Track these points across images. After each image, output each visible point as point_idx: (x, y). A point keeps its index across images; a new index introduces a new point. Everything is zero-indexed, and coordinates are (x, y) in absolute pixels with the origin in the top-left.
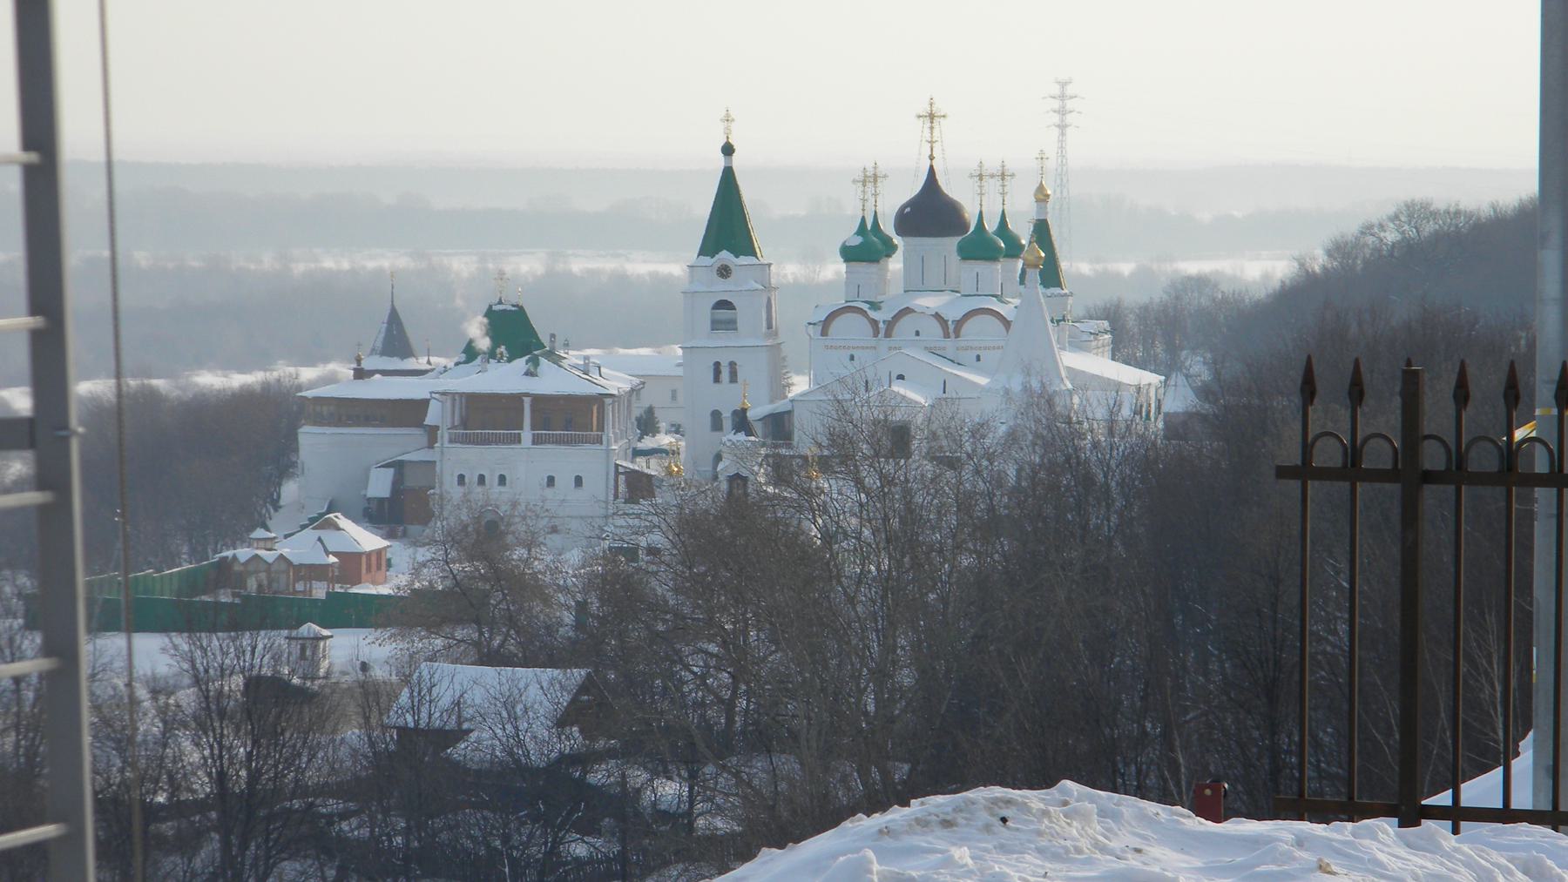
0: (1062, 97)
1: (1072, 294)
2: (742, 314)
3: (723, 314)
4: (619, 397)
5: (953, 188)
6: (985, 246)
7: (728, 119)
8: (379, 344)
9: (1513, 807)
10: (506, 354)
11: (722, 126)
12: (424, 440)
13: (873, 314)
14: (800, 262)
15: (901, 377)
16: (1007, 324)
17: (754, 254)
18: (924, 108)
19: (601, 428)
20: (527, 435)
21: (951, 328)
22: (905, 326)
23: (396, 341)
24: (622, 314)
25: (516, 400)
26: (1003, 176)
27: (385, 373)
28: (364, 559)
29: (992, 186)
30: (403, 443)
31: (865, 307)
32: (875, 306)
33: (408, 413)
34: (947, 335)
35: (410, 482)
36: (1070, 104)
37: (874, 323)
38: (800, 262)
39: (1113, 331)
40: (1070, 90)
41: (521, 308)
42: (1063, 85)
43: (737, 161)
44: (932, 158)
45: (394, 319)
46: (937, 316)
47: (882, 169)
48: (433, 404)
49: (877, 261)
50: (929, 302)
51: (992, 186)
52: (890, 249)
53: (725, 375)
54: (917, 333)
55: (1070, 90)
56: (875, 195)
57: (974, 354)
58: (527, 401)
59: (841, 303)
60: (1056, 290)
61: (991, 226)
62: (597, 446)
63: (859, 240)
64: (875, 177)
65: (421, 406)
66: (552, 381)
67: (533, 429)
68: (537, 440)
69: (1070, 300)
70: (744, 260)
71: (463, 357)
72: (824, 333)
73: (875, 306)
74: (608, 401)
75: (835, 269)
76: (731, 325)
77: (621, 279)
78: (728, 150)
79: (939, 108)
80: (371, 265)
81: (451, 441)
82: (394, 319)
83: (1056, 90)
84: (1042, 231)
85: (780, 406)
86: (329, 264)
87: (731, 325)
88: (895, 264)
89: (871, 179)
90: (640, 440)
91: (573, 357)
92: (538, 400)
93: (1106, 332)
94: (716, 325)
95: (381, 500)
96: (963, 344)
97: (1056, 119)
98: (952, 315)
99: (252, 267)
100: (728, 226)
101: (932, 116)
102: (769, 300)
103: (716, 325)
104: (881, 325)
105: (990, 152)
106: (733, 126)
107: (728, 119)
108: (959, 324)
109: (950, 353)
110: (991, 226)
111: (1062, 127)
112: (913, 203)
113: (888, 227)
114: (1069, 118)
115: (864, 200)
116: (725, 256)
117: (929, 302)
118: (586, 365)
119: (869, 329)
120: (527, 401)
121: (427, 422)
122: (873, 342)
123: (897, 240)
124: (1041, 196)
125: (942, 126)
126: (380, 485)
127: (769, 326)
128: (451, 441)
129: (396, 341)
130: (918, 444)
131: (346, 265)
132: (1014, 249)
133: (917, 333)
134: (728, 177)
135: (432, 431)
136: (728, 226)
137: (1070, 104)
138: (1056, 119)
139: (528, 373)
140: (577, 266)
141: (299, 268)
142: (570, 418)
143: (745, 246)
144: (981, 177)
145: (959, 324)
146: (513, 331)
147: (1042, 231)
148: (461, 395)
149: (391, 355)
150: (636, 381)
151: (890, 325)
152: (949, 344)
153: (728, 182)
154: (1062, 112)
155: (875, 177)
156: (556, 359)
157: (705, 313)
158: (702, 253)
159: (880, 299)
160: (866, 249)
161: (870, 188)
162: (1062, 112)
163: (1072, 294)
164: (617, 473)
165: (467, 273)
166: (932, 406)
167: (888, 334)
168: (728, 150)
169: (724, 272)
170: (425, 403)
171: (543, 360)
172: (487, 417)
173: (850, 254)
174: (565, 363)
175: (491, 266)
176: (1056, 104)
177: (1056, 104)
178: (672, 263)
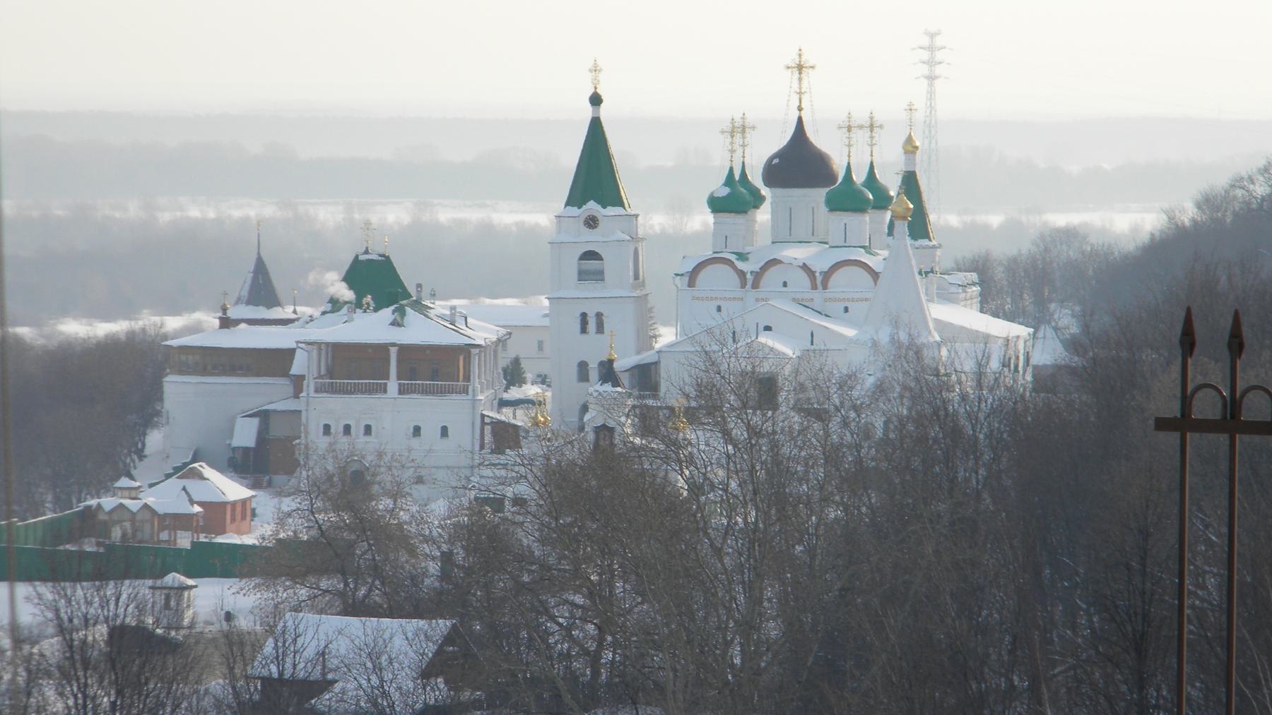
1: (940, 246)
2: (610, 264)
3: (592, 264)
6: (852, 197)
7: (595, 69)
8: (245, 293)
9: (1177, 435)
11: (590, 76)
12: (290, 390)
13: (741, 265)
14: (667, 213)
15: (768, 328)
16: (875, 275)
17: (620, 203)
18: (792, 59)
19: (467, 378)
20: (393, 385)
21: (820, 280)
22: (772, 278)
23: (262, 289)
24: (490, 264)
25: (382, 349)
26: (872, 127)
29: (861, 137)
30: (269, 393)
31: (733, 258)
32: (742, 257)
33: (274, 362)
34: (814, 287)
36: (939, 56)
37: (742, 274)
38: (667, 213)
40: (939, 41)
41: (388, 258)
42: (932, 36)
43: (605, 112)
44: (800, 109)
45: (260, 269)
46: (805, 267)
47: (750, 120)
52: (758, 200)
54: (785, 284)
55: (939, 41)
56: (744, 146)
57: (842, 305)
58: (393, 351)
59: (709, 254)
60: (925, 242)
61: (859, 177)
62: (463, 397)
63: (726, 191)
65: (289, 354)
67: (399, 378)
69: (939, 252)
70: (611, 211)
72: (691, 284)
73: (742, 257)
74: (474, 351)
75: (702, 220)
76: (598, 276)
78: (596, 100)
79: (808, 59)
80: (237, 214)
81: (316, 391)
82: (260, 269)
83: (926, 41)
84: (910, 183)
85: (647, 357)
86: (194, 213)
87: (598, 276)
88: (763, 215)
89: (739, 130)
91: (440, 307)
92: (406, 351)
93: (974, 284)
94: (583, 275)
95: (246, 450)
96: (831, 295)
97: (925, 70)
98: (820, 266)
100: (595, 177)
101: (800, 68)
103: (583, 275)
104: (749, 276)
105: (859, 105)
106: (601, 76)
107: (595, 69)
108: (827, 275)
109: (817, 304)
110: (859, 177)
111: (931, 78)
112: (781, 154)
113: (756, 179)
114: (938, 70)
116: (592, 207)
118: (453, 315)
120: (393, 351)
121: (292, 372)
122: (739, 293)
123: (765, 191)
124: (910, 148)
125: (810, 77)
126: (245, 434)
127: (636, 277)
128: (316, 391)
131: (212, 215)
132: (882, 200)
133: (785, 284)
135: (298, 381)
136: (595, 177)
138: (925, 70)
139: (395, 323)
140: (445, 216)
141: (165, 217)
142: (435, 368)
143: (612, 196)
144: (849, 129)
145: (827, 275)
146: (376, 280)
148: (327, 344)
150: (503, 331)
151: (758, 276)
152: (818, 296)
153: (596, 131)
156: (419, 307)
157: (571, 265)
158: (569, 203)
159: (747, 249)
160: (734, 200)
162: (931, 63)
163: (940, 246)
164: (483, 423)
167: (755, 285)
168: (596, 100)
169: (592, 222)
170: (291, 352)
171: (408, 309)
172: (353, 367)
173: (717, 205)
175: (357, 216)
176: (925, 55)
177: (925, 55)
178: (541, 213)
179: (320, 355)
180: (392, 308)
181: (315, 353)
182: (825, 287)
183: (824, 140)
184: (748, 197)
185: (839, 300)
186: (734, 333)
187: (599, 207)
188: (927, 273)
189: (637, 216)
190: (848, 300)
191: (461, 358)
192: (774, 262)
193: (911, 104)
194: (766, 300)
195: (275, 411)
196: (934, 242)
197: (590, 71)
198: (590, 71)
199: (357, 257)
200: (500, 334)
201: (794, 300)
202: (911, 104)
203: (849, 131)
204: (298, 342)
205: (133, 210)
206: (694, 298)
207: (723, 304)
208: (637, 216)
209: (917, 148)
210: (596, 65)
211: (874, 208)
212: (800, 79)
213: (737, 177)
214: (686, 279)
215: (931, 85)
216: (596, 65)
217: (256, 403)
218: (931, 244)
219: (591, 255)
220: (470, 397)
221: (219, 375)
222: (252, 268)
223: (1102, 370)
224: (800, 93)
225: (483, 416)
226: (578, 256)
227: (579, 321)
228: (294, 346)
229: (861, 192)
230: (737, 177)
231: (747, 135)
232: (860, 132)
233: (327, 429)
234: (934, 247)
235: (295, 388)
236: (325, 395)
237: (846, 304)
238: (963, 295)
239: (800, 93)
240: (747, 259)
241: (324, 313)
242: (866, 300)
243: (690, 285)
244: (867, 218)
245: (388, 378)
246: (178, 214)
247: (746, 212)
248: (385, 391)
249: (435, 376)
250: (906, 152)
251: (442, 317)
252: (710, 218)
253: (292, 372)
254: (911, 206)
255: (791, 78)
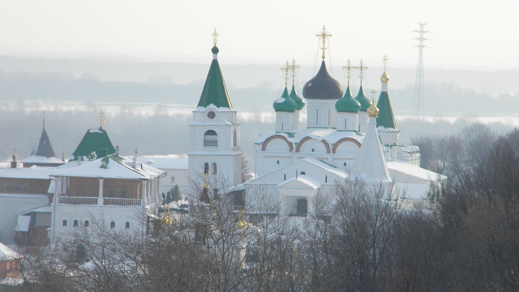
0: (422, 32)
1: (399, 132)
2: (220, 138)
3: (211, 137)
4: (151, 180)
5: (333, 74)
6: (349, 105)
7: (215, 34)
8: (36, 149)
10: (95, 155)
11: (212, 37)
12: (47, 201)
13: (290, 139)
14: (252, 112)
15: (303, 173)
16: (359, 144)
17: (227, 105)
18: (320, 31)
19: (141, 197)
20: (101, 200)
21: (331, 148)
22: (307, 147)
23: (45, 148)
24: (155, 137)
25: (95, 180)
27: (39, 165)
28: (8, 264)
29: (355, 73)
30: (35, 202)
31: (286, 136)
32: (291, 135)
33: (39, 186)
34: (329, 152)
35: (39, 223)
36: (425, 35)
37: (290, 144)
38: (252, 112)
39: (421, 152)
40: (425, 28)
41: (105, 132)
42: (422, 25)
43: (220, 57)
44: (323, 57)
45: (44, 136)
46: (324, 141)
47: (297, 63)
48: (52, 183)
49: (292, 111)
50: (320, 134)
51: (355, 73)
52: (300, 105)
53: (211, 168)
54: (313, 150)
55: (425, 28)
56: (294, 76)
57: (276, 160)
58: (101, 182)
59: (274, 133)
60: (391, 129)
61: (354, 94)
62: (138, 207)
63: (283, 100)
64: (294, 67)
65: (46, 183)
66: (116, 171)
67: (104, 196)
68: (106, 203)
69: (398, 135)
70: (222, 109)
71: (73, 157)
72: (264, 149)
73: (291, 135)
74: (145, 182)
75: (269, 115)
76: (214, 143)
77: (70, 112)
78: (215, 50)
79: (328, 31)
80: (65, 109)
81: (60, 202)
82: (44, 136)
83: (418, 28)
84: (384, 97)
85: (241, 186)
86: (44, 108)
87: (214, 143)
88: (303, 115)
89: (291, 68)
90: (163, 204)
91: (128, 159)
92: (108, 181)
93: (417, 152)
94: (207, 143)
95: (23, 233)
96: (338, 157)
97: (418, 43)
98: (332, 141)
99: (4, 109)
100: (214, 90)
101: (324, 36)
102: (235, 131)
103: (207, 143)
104: (294, 145)
105: (358, 56)
106: (218, 38)
107: (215, 34)
109: (330, 161)
110: (354, 94)
111: (421, 47)
112: (312, 81)
113: (299, 94)
114: (425, 43)
115: (286, 79)
116: (212, 107)
117: (320, 134)
118: (134, 163)
119: (287, 147)
120: (101, 182)
121: (48, 192)
122: (289, 154)
123: (304, 100)
124: (385, 79)
126: (23, 224)
127: (235, 145)
128: (60, 202)
129: (45, 148)
130: (311, 208)
131: (52, 109)
132: (366, 105)
133: (313, 150)
134: (215, 65)
135: (51, 196)
136: (214, 90)
137: (425, 35)
138: (418, 43)
139: (103, 167)
140: (171, 112)
141: (28, 110)
142: (123, 191)
143: (223, 102)
144: (349, 68)
145: (336, 145)
146: (97, 144)
147: (384, 97)
148: (67, 177)
149: (42, 155)
150: (162, 172)
151: (299, 145)
152: (330, 157)
154: (421, 39)
155: (294, 67)
156: (117, 159)
157: (201, 137)
158: (200, 104)
159: (294, 131)
160: (287, 105)
161: (290, 72)
162: (421, 39)
163: (399, 132)
164: (148, 221)
165: (76, 113)
166: (319, 189)
167: (298, 150)
168: (215, 50)
169: (212, 115)
170: (48, 181)
171: (110, 160)
172: (81, 190)
173: (278, 107)
174: (123, 162)
175: (126, 111)
176: (418, 35)
177: (418, 35)
178: (185, 109)
179: (62, 183)
180: (102, 158)
181: (60, 182)
182: (334, 151)
183: (335, 74)
184: (295, 104)
185: (342, 159)
186: (326, 176)
187: (215, 107)
188: (391, 146)
189: (236, 112)
190: (346, 159)
191: (139, 185)
192: (307, 138)
193: (385, 56)
194: (304, 158)
195: (40, 213)
196: (396, 130)
197: (213, 35)
198: (213, 35)
199: (89, 131)
200: (160, 173)
201: (317, 158)
202: (385, 56)
203: (361, 70)
204: (50, 176)
205: (13, 107)
206: (265, 156)
207: (347, 162)
208: (236, 112)
209: (388, 79)
210: (215, 32)
211: (361, 111)
212: (324, 42)
213: (289, 93)
214: (261, 146)
215: (421, 51)
216: (215, 32)
217: (29, 208)
218: (394, 130)
219: (211, 133)
220: (141, 207)
221: (9, 192)
222: (40, 136)
223: (452, 203)
224: (324, 49)
225: (149, 217)
226: (204, 132)
227: (203, 166)
228: (48, 178)
229: (354, 102)
230: (289, 93)
231: (296, 70)
232: (355, 70)
233: (65, 223)
234: (396, 132)
235: (50, 200)
236: (64, 204)
237: (345, 161)
238: (410, 158)
239: (324, 49)
240: (294, 137)
241: (70, 161)
242: (354, 159)
243: (262, 150)
244: (357, 116)
245: (98, 196)
246: (35, 109)
247: (293, 111)
248: (96, 203)
249: (123, 195)
250: (382, 82)
251: (128, 164)
252: (275, 114)
253: (48, 192)
254: (378, 110)
255: (318, 41)
